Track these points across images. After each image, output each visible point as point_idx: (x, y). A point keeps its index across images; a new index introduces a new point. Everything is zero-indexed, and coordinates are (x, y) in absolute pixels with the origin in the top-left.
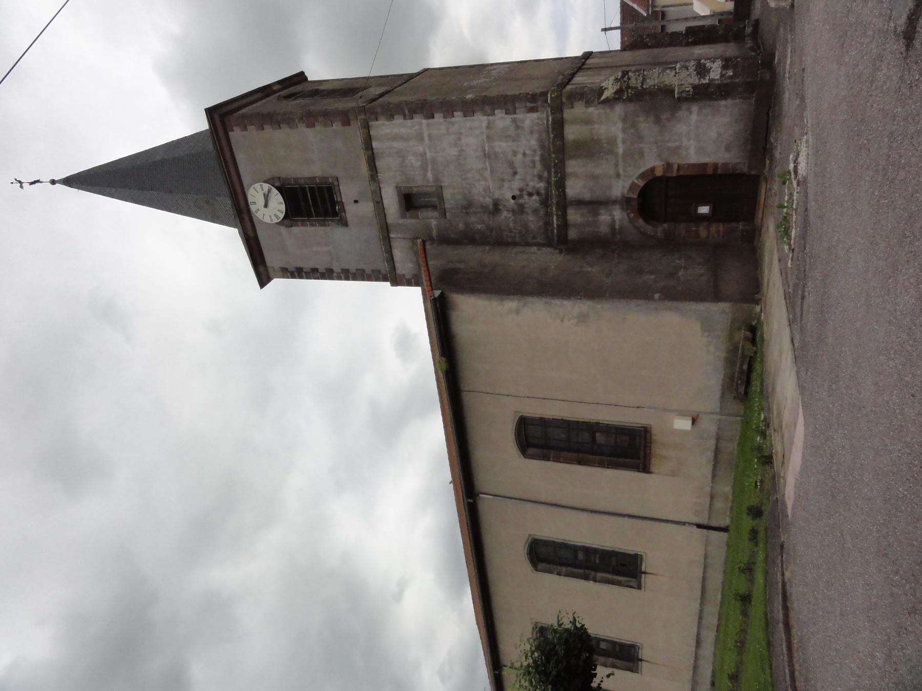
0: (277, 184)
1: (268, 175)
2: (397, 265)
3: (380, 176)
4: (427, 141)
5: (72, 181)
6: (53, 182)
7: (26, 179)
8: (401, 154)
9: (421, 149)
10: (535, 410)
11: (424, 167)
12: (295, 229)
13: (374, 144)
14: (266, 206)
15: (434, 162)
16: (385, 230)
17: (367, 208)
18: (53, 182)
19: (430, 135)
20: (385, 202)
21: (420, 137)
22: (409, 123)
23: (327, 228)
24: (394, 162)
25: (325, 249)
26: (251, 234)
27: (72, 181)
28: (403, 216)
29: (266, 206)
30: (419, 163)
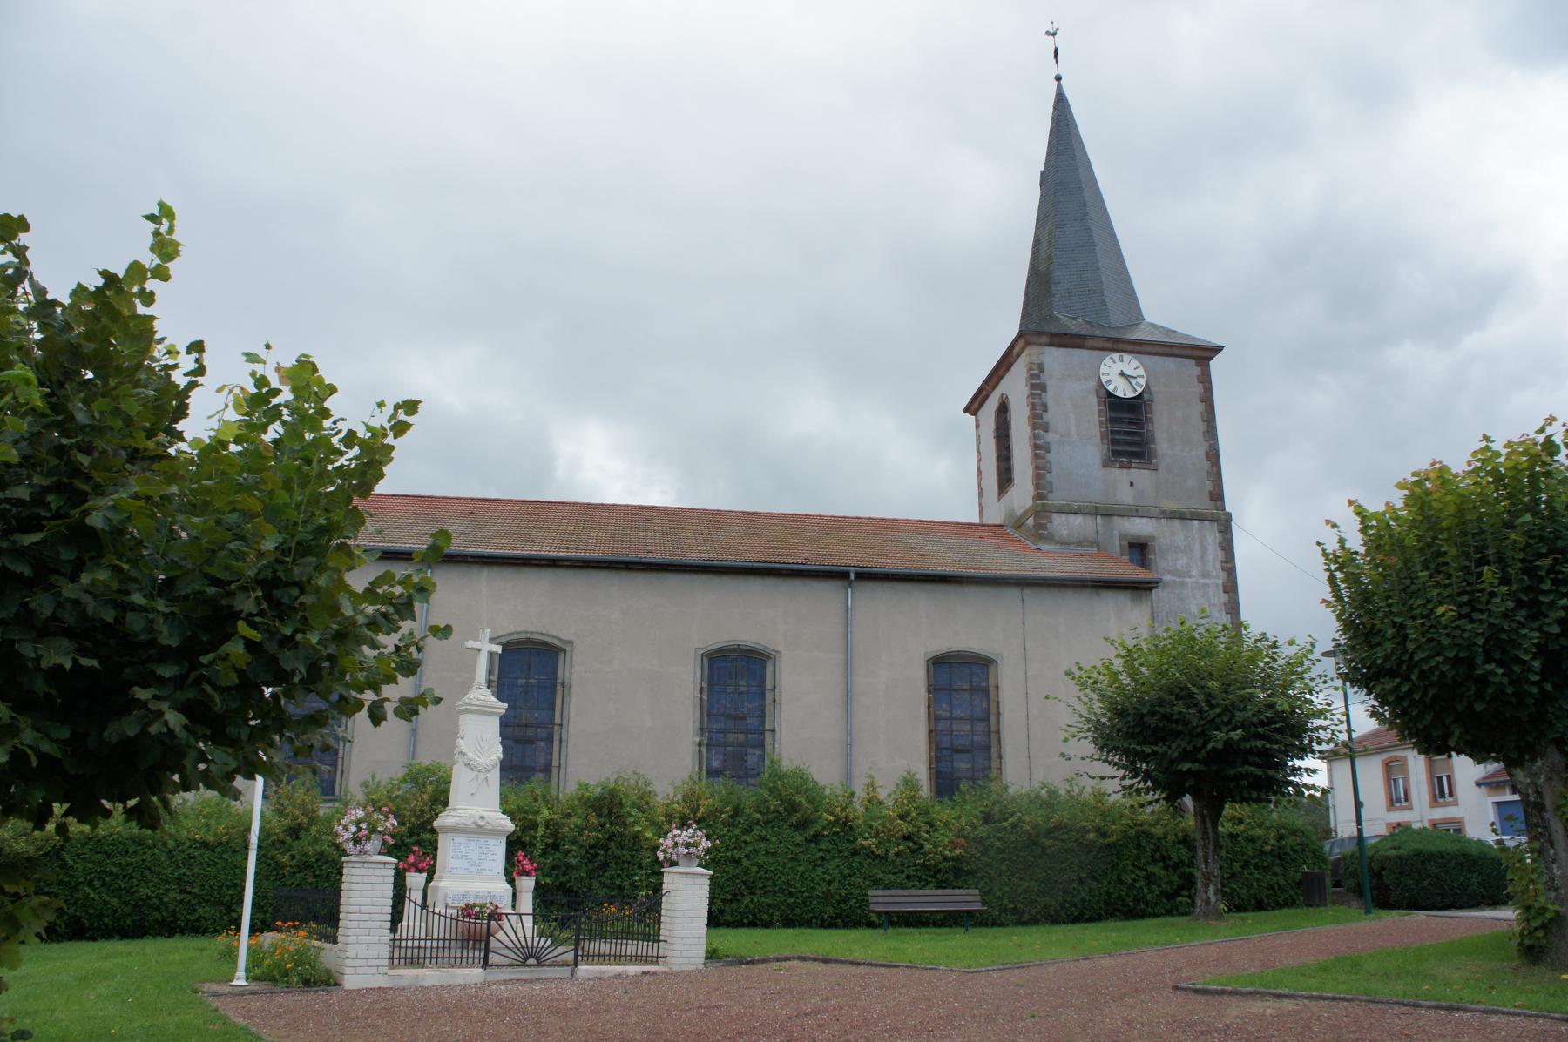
0: (1146, 397)
1: (1154, 389)
2: (1064, 517)
3: (1164, 521)
4: (1202, 581)
5: (1061, 102)
6: (1058, 79)
7: (1060, 40)
8: (1187, 550)
9: (1194, 573)
10: (579, 671)
11: (1175, 572)
12: (1094, 400)
13: (1196, 523)
14: (1122, 374)
15: (1182, 585)
16: (1105, 512)
17: (1125, 496)
18: (1058, 79)
19: (1207, 585)
20: (1137, 520)
21: (1205, 574)
22: (1219, 565)
23: (1098, 440)
24: (1180, 540)
25: (1073, 430)
26: (1089, 343)
27: (1061, 102)
28: (1122, 537)
29: (1122, 374)
30: (96, 520)
